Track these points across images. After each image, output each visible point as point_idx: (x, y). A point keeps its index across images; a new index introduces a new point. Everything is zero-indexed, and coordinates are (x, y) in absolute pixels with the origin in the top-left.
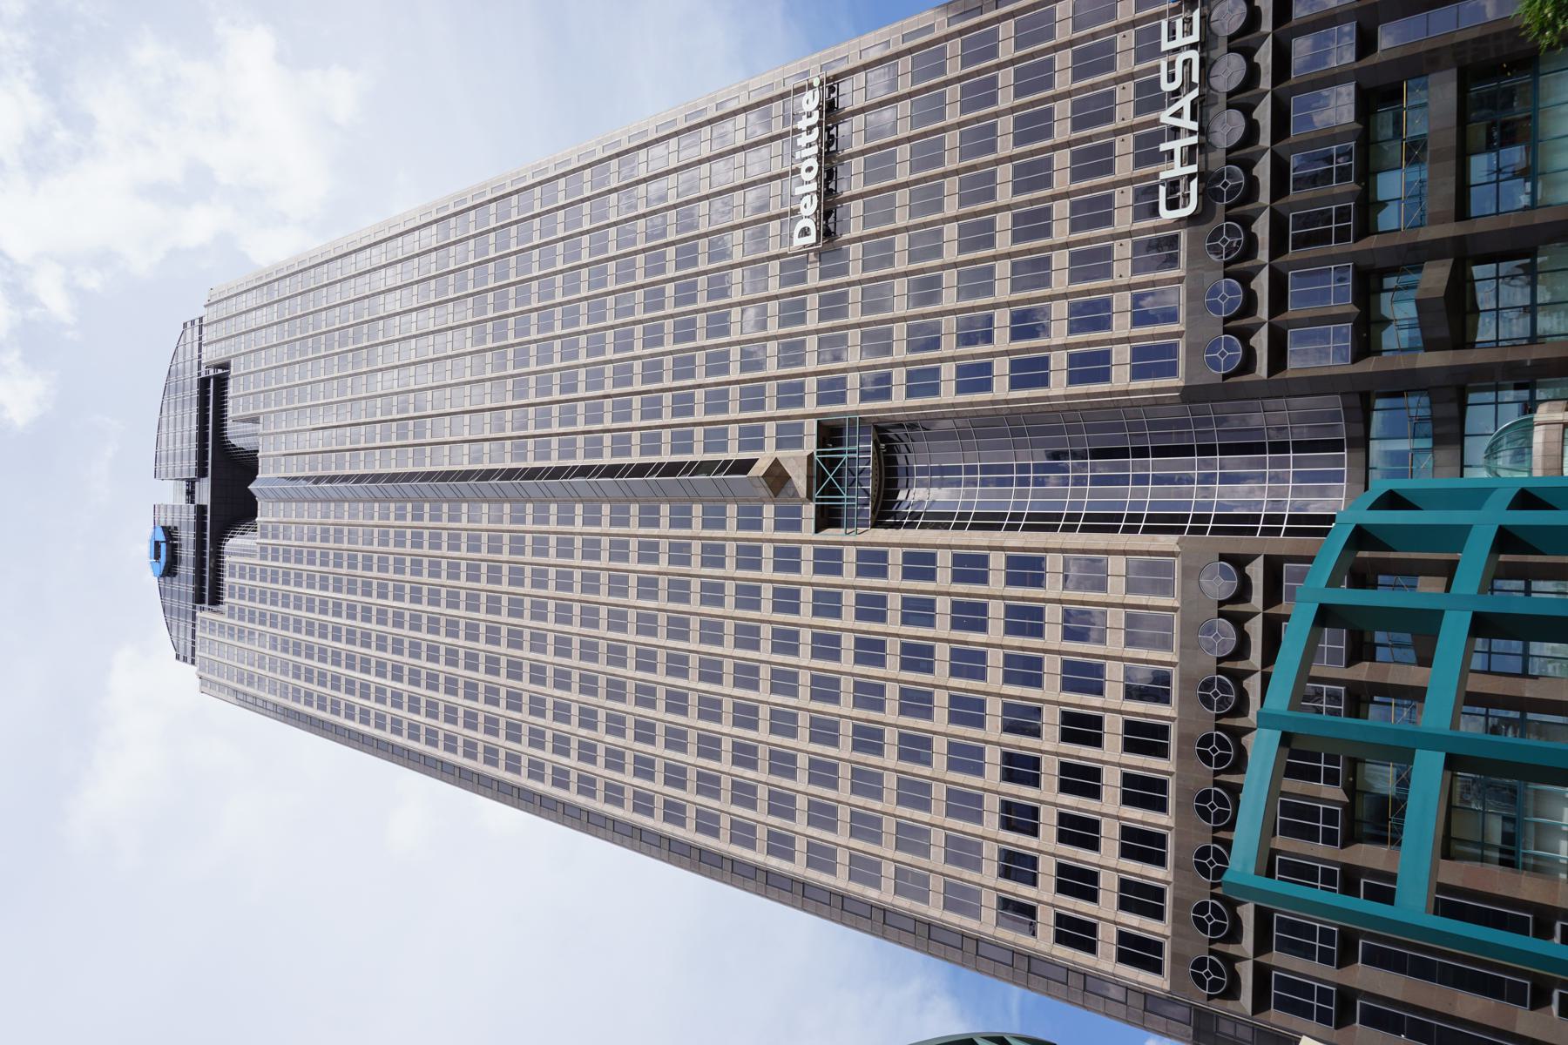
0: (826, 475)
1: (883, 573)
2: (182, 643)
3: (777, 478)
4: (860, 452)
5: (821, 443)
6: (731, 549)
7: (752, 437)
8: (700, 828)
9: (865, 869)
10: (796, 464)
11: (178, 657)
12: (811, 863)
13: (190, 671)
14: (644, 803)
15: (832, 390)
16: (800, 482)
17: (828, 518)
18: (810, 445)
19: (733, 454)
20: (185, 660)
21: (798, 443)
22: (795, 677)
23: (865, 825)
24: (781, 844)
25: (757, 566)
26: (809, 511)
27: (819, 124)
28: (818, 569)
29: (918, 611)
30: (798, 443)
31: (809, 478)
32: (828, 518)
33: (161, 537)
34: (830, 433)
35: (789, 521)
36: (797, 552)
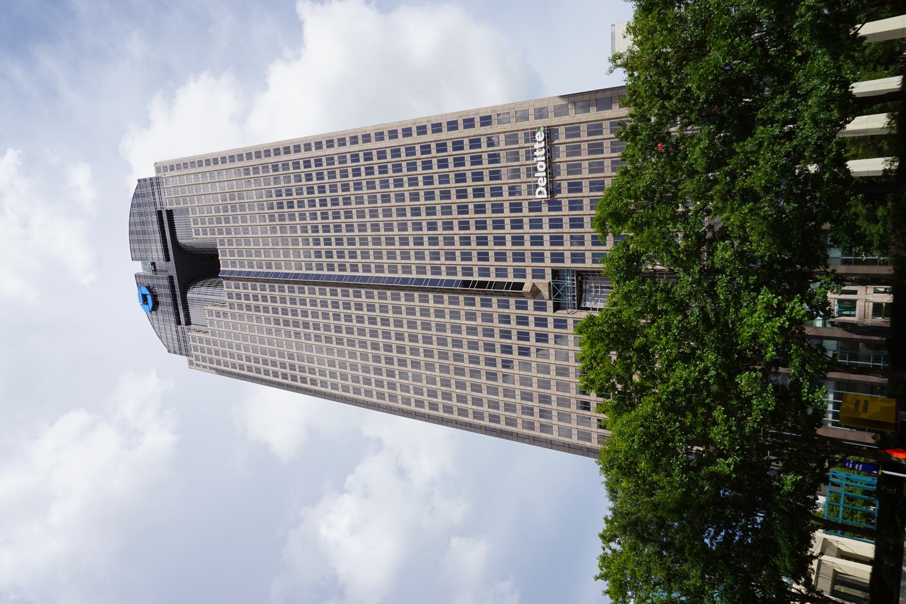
0: (556, 290)
1: (466, 197)
2: (171, 345)
3: (535, 292)
4: (569, 282)
5: (553, 278)
6: (367, 211)
7: (520, 273)
8: (302, 382)
9: (368, 393)
10: (543, 285)
11: (169, 351)
12: (507, 424)
13: (184, 359)
14: (285, 376)
15: (557, 257)
16: (545, 293)
17: (557, 307)
18: (549, 278)
19: (511, 279)
20: (175, 353)
21: (543, 277)
22: (383, 267)
23: (415, 364)
24: (393, 398)
25: (363, 203)
26: (550, 304)
27: (545, 147)
28: (395, 186)
29: (499, 224)
30: (543, 277)
31: (550, 292)
32: (557, 307)
33: (146, 292)
34: (556, 273)
35: (541, 307)
36: (403, 195)
